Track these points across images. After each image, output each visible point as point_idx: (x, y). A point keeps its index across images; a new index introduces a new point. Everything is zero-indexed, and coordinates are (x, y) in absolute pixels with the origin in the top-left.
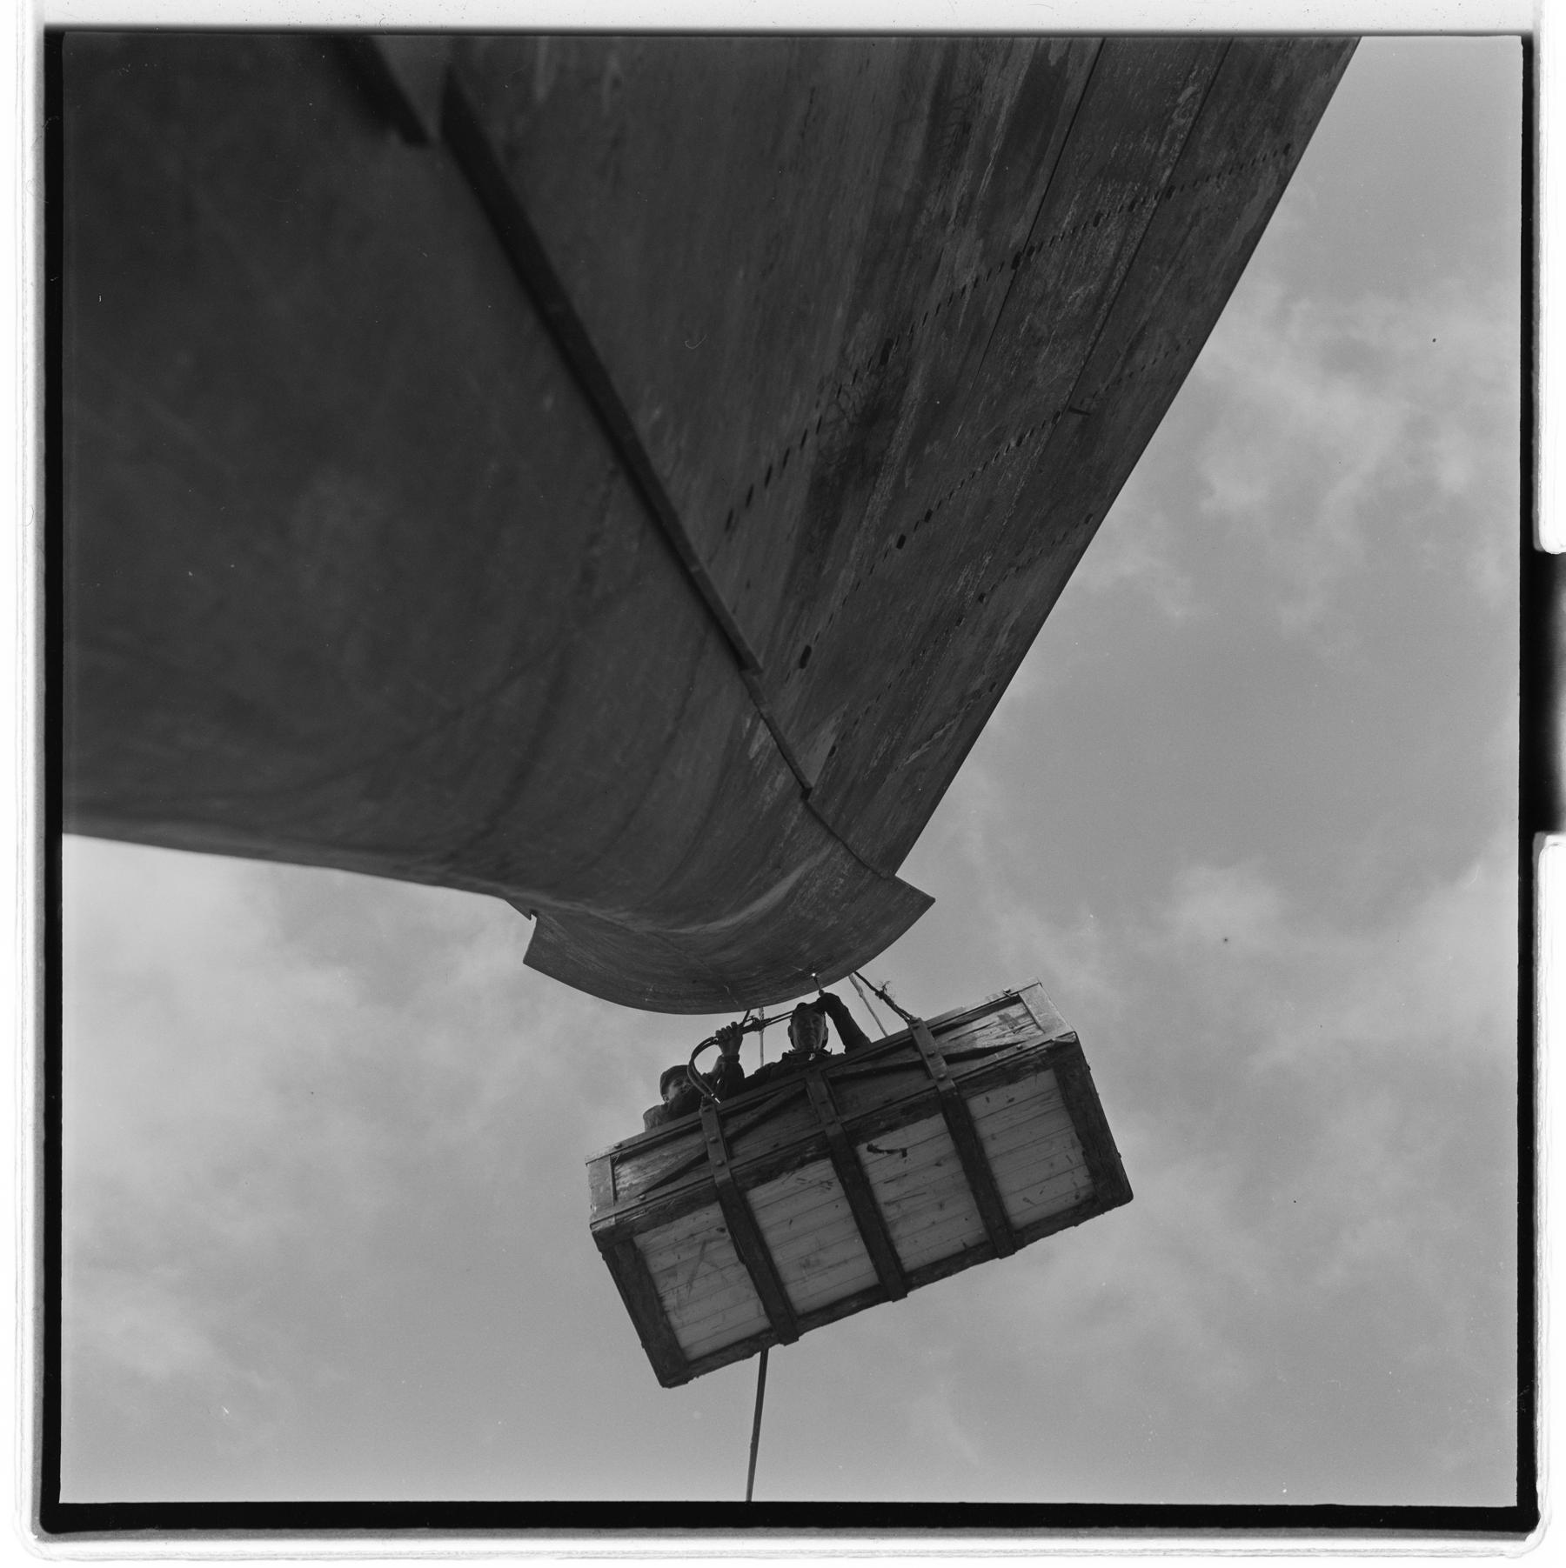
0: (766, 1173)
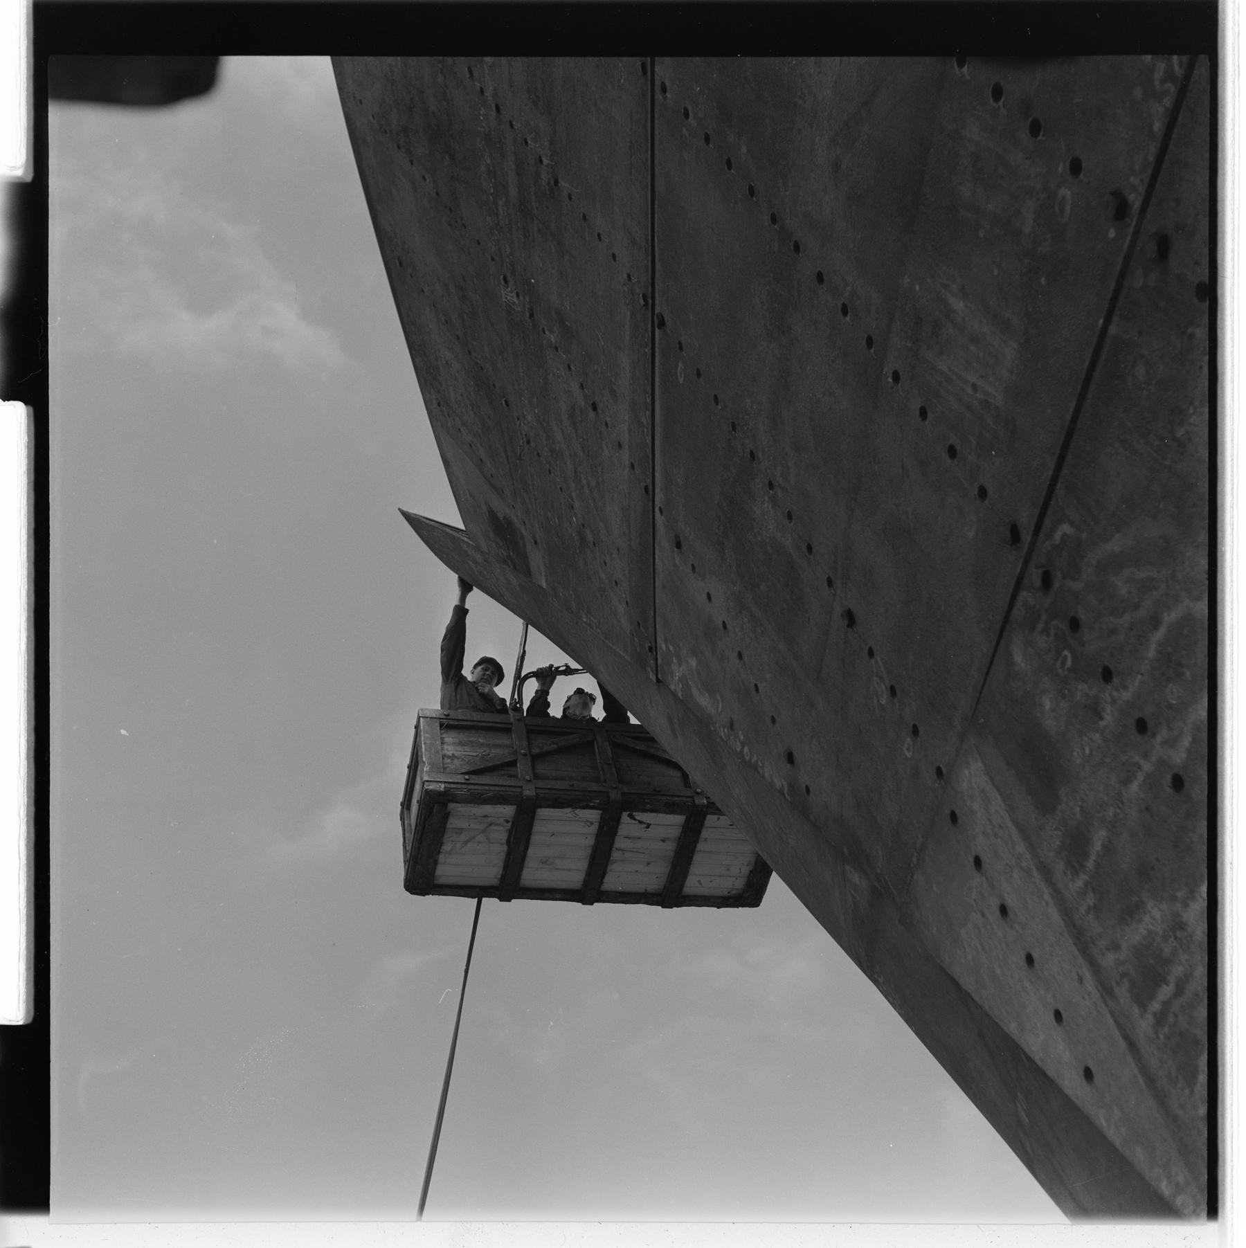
0: (557, 803)
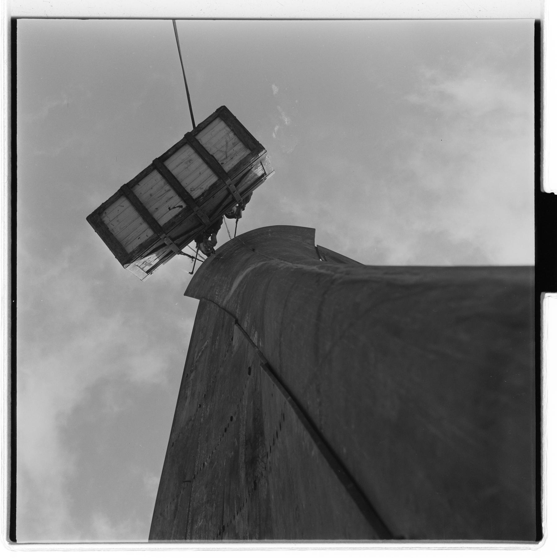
0: (214, 187)
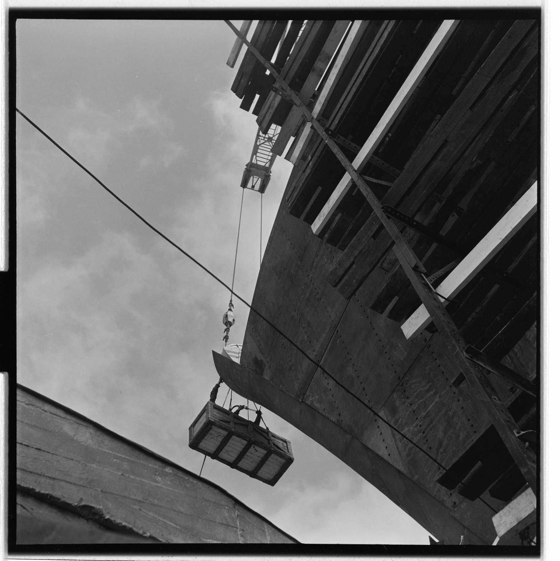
0: (239, 436)
